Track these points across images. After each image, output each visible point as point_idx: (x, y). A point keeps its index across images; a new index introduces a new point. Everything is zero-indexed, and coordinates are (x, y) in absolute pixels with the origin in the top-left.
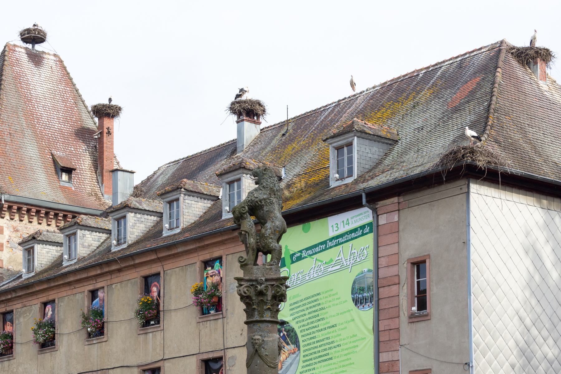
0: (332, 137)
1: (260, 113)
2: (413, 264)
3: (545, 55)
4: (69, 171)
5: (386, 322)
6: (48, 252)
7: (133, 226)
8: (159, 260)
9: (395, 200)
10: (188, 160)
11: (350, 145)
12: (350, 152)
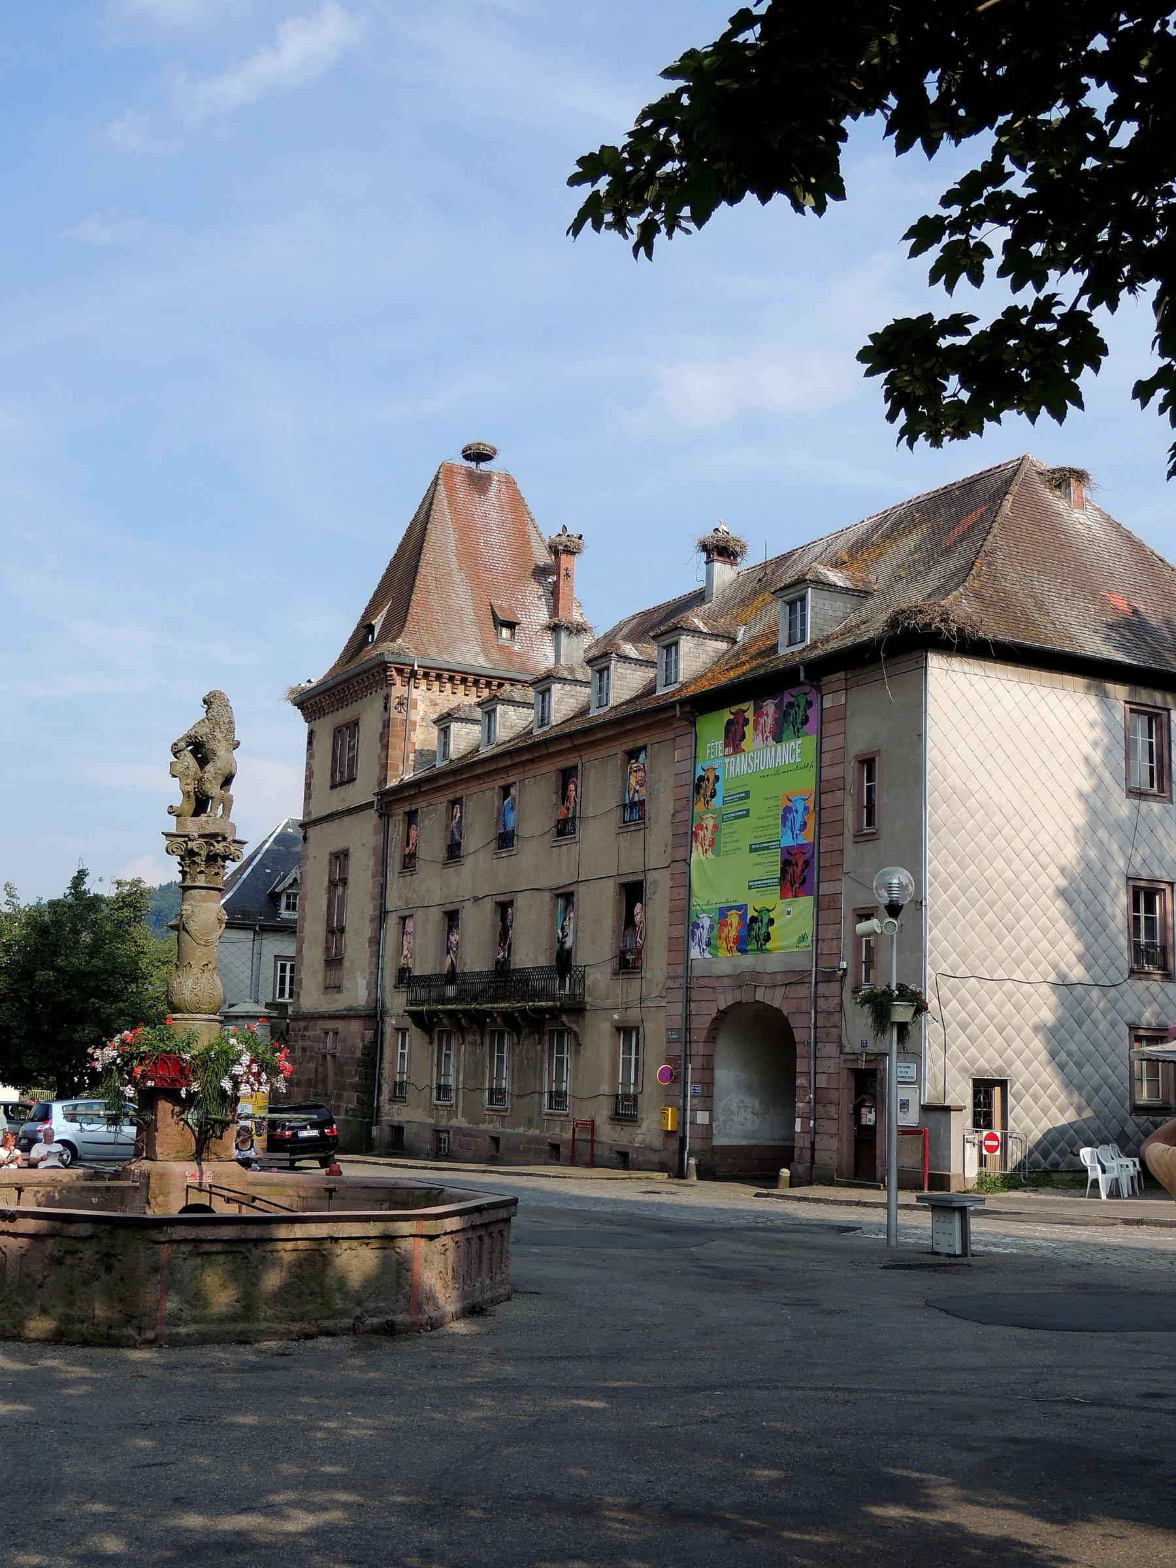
0: (781, 589)
1: (738, 550)
2: (862, 762)
3: (1080, 476)
4: (511, 625)
5: (829, 841)
6: (468, 734)
7: (559, 702)
8: (576, 749)
9: (842, 675)
10: (655, 610)
11: (803, 599)
12: (803, 609)
